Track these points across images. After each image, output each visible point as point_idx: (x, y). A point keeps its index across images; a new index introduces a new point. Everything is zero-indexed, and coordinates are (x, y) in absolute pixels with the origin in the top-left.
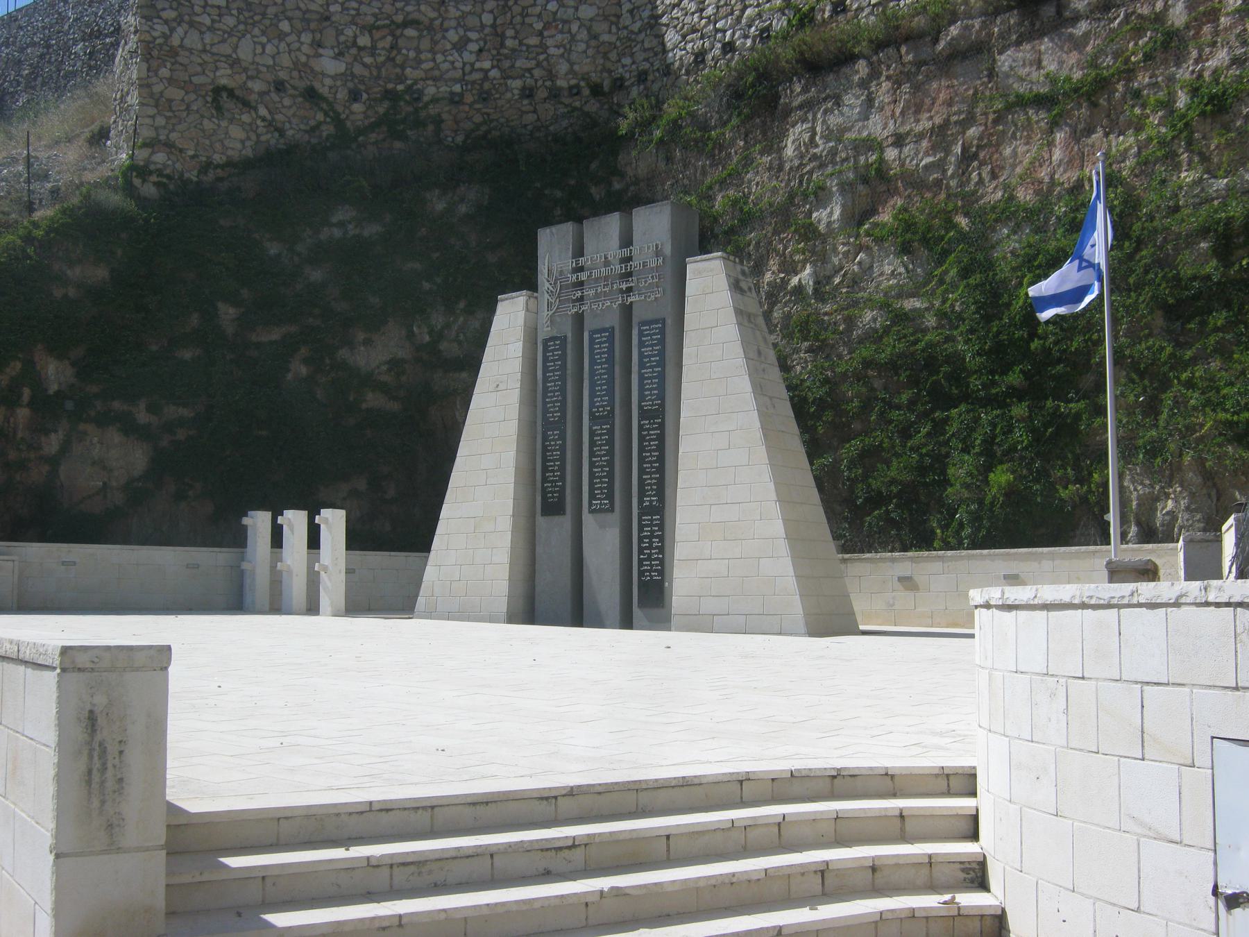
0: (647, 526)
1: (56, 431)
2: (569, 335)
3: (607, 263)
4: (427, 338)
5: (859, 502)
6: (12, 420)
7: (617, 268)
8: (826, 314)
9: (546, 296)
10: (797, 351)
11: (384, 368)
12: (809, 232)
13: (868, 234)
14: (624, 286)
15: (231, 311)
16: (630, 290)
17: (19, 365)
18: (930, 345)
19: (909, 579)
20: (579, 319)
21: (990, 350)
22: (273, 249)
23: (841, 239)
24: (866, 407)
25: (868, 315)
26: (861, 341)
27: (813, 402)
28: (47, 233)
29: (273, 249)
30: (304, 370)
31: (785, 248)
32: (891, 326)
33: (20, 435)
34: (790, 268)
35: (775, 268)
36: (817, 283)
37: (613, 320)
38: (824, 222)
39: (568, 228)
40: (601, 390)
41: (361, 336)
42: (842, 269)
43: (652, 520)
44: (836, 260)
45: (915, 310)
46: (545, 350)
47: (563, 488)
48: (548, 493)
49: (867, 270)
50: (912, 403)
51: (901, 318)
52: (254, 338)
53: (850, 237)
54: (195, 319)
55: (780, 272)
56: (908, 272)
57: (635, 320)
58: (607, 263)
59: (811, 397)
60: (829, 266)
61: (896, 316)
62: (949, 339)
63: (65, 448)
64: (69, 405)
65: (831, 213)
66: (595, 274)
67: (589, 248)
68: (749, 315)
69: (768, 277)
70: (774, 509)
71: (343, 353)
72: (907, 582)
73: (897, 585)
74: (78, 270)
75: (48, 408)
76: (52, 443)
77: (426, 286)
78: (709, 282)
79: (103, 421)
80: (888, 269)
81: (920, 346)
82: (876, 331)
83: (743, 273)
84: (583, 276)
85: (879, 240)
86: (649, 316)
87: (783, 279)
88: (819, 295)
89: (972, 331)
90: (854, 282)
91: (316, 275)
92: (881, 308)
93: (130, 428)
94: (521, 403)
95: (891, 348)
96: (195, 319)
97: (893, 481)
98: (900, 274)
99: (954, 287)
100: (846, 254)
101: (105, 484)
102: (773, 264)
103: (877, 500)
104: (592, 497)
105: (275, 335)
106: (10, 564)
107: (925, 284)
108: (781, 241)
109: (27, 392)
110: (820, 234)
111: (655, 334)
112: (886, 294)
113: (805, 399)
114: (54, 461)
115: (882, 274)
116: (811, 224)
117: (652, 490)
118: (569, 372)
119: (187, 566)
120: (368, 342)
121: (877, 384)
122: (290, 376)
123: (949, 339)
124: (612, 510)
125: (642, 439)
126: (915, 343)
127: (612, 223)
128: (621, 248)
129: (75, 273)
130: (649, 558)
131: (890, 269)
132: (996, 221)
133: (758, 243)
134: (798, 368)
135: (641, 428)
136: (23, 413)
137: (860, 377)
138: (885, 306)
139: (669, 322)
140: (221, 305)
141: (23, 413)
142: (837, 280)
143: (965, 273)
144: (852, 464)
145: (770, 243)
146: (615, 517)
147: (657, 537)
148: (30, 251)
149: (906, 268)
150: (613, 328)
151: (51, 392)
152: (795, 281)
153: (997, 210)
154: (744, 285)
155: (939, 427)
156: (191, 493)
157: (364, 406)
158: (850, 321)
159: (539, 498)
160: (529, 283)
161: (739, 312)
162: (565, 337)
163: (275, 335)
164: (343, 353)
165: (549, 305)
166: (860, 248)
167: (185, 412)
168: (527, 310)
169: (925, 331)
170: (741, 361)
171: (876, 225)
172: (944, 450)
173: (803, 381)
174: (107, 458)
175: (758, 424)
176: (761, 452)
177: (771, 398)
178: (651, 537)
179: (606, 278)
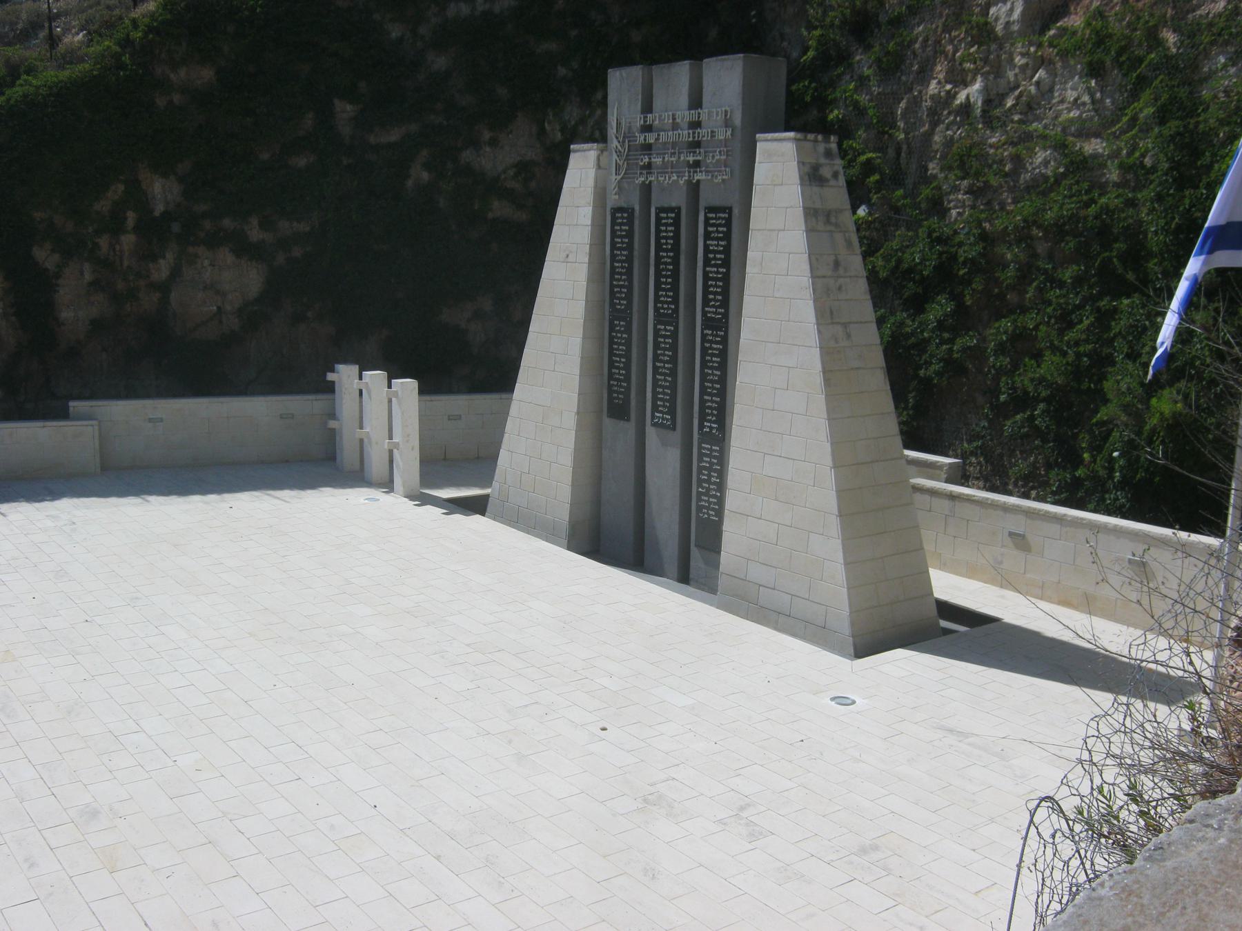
0: (707, 455)
1: (164, 257)
2: (637, 208)
3: (675, 126)
4: (559, 136)
5: (1003, 398)
6: (118, 247)
7: (685, 135)
8: (991, 146)
9: (615, 156)
10: (956, 189)
11: (511, 172)
12: (984, 34)
13: (1051, 45)
14: (691, 159)
15: (349, 107)
16: (697, 164)
17: (121, 187)
18: (1106, 209)
19: (1023, 536)
20: (647, 189)
21: (1179, 226)
22: (395, 31)
23: (1019, 48)
24: (1025, 275)
25: (1040, 156)
26: (1028, 189)
27: (964, 263)
28: (146, 34)
29: (395, 31)
30: (425, 176)
31: (956, 50)
32: (1064, 175)
33: (126, 263)
34: (959, 78)
35: (941, 76)
36: (988, 102)
37: (678, 199)
38: (1002, 21)
39: (636, 72)
40: (666, 283)
41: (487, 135)
42: (1017, 87)
43: (711, 450)
44: (1011, 75)
45: (1095, 156)
46: (614, 219)
47: (628, 389)
48: (614, 394)
49: (1046, 91)
50: (1079, 281)
51: (1080, 166)
52: (372, 140)
53: (1031, 44)
54: (309, 120)
55: (947, 82)
56: (1093, 102)
57: (703, 204)
58: (675, 126)
59: (962, 254)
60: (1002, 82)
61: (1072, 163)
62: (1131, 203)
63: (176, 273)
64: (176, 227)
65: (1012, 10)
66: (670, 136)
67: (658, 104)
68: (828, 214)
69: (933, 87)
70: (828, 477)
71: (467, 156)
72: (1020, 541)
73: (1008, 541)
74: (182, 72)
75: (154, 231)
76: (161, 270)
77: (562, 71)
78: (779, 162)
79: (213, 241)
80: (1071, 95)
81: (1092, 210)
82: (1046, 178)
83: (828, 154)
84: (651, 138)
85: (1064, 54)
86: (717, 202)
87: (948, 92)
88: (989, 120)
89: (1159, 198)
90: (1030, 108)
91: (440, 62)
92: (1055, 148)
93: (245, 249)
94: (590, 280)
95: (1056, 208)
96: (309, 120)
97: (1042, 380)
98: (1084, 104)
99: (1146, 130)
100: (1023, 68)
101: (219, 308)
102: (940, 69)
103: (1022, 401)
104: (655, 408)
105: (394, 136)
106: (90, 429)
107: (1113, 123)
108: (951, 41)
109: (131, 217)
110: (996, 38)
111: (720, 225)
112: (1064, 130)
113: (954, 257)
114: (164, 288)
115: (1062, 102)
116: (986, 23)
117: (712, 415)
118: (636, 253)
119: (281, 417)
120: (494, 142)
121: (1042, 248)
122: (410, 183)
123: (1131, 203)
124: (674, 429)
125: (704, 351)
126: (1087, 205)
127: (681, 72)
128: (690, 108)
129: (180, 76)
130: (707, 494)
131: (1073, 95)
132: (1212, 43)
133: (926, 40)
134: (954, 212)
135: (704, 336)
136: (128, 240)
137: (1023, 236)
138: (1061, 147)
139: (736, 211)
140: (336, 101)
141: (128, 240)
142: (1010, 103)
143: (1162, 117)
144: (1001, 349)
145: (938, 42)
146: (676, 436)
147: (715, 471)
148: (126, 58)
149: (1092, 96)
150: (679, 209)
151: (157, 214)
152: (961, 97)
153: (1214, 30)
154: (826, 172)
155: (1105, 318)
156: (309, 314)
157: (490, 215)
158: (1017, 160)
159: (605, 396)
160: (598, 136)
161: (810, 213)
162: (633, 209)
163: (394, 136)
164: (467, 156)
165: (618, 168)
166: (1042, 62)
167: (303, 227)
168: (599, 167)
169: (1103, 188)
170: (806, 281)
171: (1064, 30)
172: (1106, 351)
173: (956, 232)
174: (220, 283)
175: (819, 367)
176: (820, 400)
177: (845, 325)
178: (710, 469)
179: (674, 145)
